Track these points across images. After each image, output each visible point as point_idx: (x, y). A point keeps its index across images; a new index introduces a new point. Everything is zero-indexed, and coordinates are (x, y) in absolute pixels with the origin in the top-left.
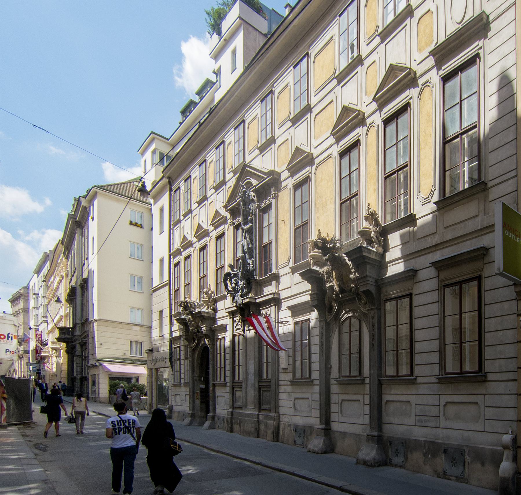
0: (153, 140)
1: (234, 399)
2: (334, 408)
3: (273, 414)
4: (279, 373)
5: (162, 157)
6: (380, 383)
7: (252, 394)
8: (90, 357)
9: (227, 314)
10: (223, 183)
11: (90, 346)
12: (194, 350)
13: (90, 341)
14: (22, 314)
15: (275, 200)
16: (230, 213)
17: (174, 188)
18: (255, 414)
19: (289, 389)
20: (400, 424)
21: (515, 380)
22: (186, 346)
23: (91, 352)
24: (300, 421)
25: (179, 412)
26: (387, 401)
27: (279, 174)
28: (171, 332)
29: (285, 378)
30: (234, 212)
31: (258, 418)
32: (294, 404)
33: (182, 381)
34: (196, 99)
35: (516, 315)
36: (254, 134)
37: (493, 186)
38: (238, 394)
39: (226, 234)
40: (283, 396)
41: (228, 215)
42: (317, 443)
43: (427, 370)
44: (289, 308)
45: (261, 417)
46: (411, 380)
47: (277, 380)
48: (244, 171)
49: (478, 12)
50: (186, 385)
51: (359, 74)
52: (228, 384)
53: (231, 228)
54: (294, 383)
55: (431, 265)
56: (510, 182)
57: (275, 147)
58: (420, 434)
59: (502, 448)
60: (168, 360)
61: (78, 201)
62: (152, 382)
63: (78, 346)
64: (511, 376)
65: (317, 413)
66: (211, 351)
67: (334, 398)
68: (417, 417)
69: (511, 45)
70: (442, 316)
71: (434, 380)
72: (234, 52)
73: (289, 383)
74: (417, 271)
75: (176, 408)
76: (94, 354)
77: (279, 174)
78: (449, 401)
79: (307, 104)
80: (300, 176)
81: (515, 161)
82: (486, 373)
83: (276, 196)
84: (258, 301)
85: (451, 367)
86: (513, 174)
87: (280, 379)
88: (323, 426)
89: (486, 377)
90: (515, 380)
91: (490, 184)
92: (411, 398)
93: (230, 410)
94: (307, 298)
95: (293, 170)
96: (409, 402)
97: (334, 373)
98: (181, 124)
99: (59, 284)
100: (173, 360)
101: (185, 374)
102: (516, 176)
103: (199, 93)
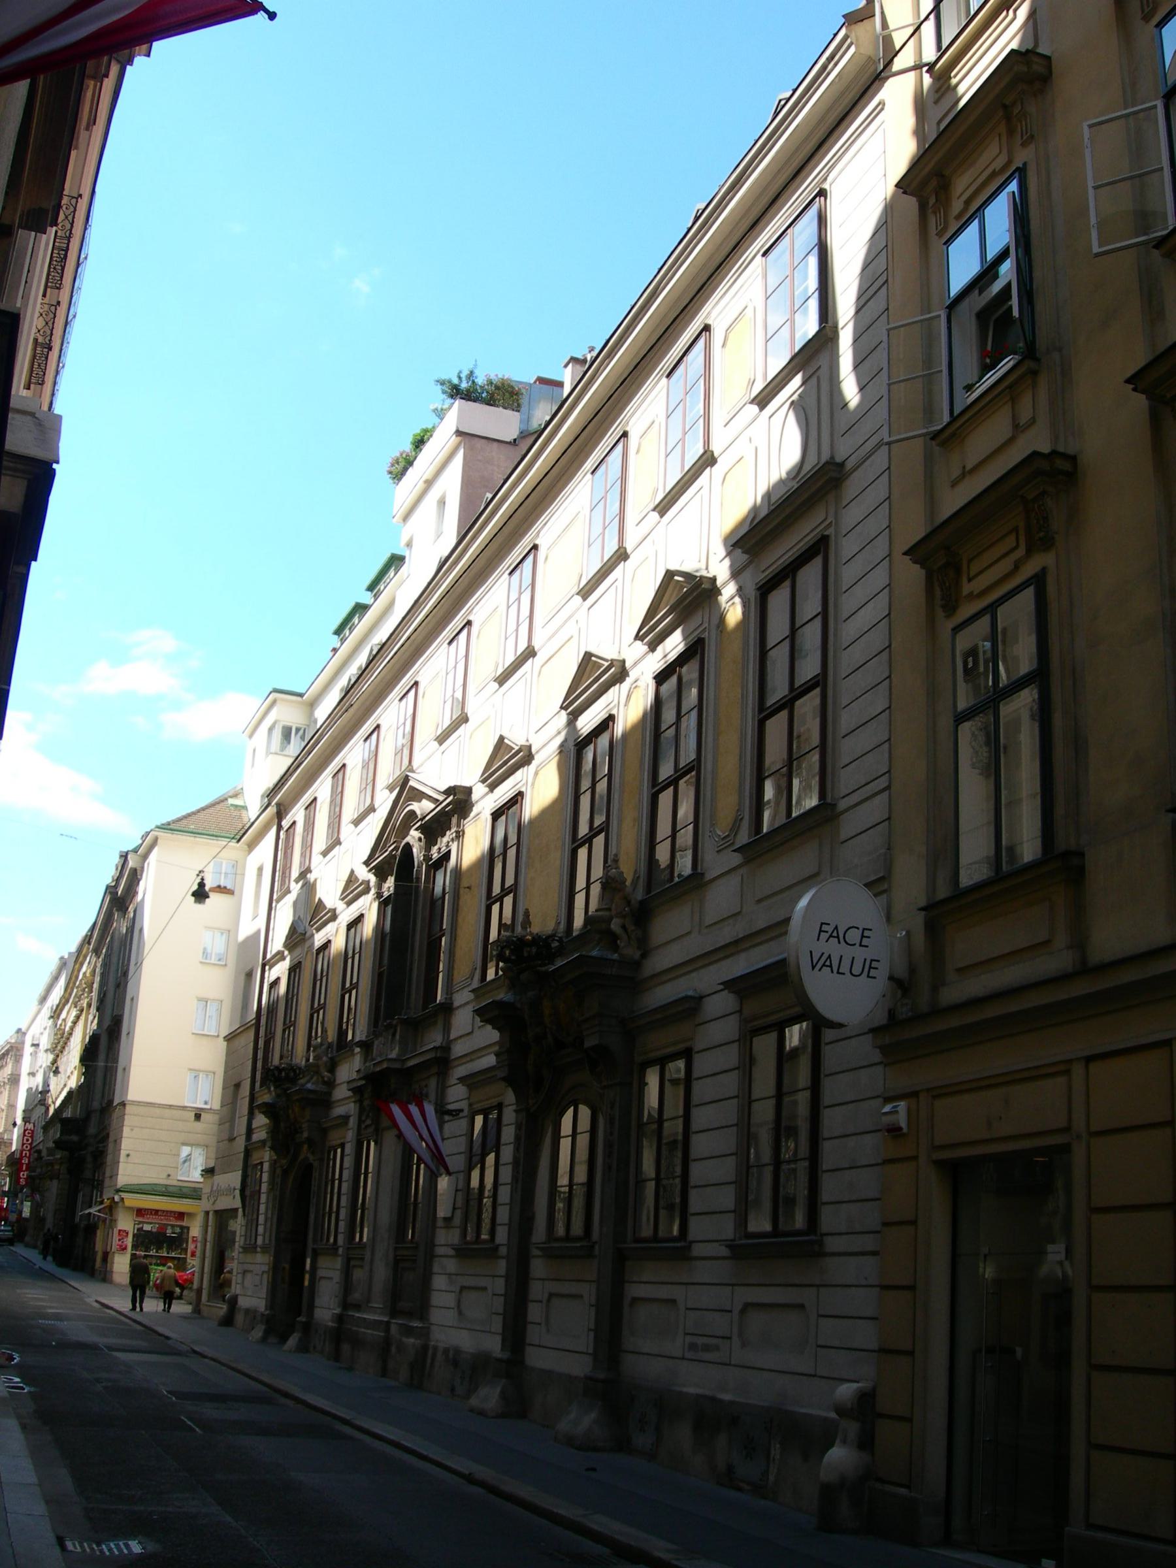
0: (274, 702)
1: (347, 1285)
2: (534, 1312)
3: (416, 1324)
4: (434, 1227)
5: (287, 733)
6: (621, 1259)
7: (382, 1273)
8: (107, 1182)
9: (350, 1093)
10: (371, 809)
11: (109, 1158)
12: (286, 1172)
13: (111, 1146)
14: (8, 1087)
15: (456, 843)
16: (375, 875)
17: (286, 823)
18: (381, 1322)
19: (451, 1265)
20: (660, 1357)
21: (874, 1253)
22: (273, 1164)
23: (108, 1174)
24: (466, 1342)
25: (247, 1311)
26: (635, 1300)
27: (468, 791)
28: (250, 1131)
29: (446, 1239)
30: (381, 873)
31: (387, 1330)
32: (459, 1301)
33: (260, 1241)
34: (367, 598)
35: (881, 1100)
36: (434, 712)
37: (846, 810)
38: (358, 1274)
39: (366, 917)
40: (439, 1282)
41: (373, 879)
42: (489, 1396)
43: (711, 1229)
44: (462, 1080)
45: (394, 1329)
46: (679, 1251)
47: (431, 1245)
48: (405, 789)
49: (825, 457)
50: (265, 1249)
51: (528, 676)
52: (340, 1251)
53: (375, 905)
54: (463, 1252)
55: (721, 987)
56: (877, 800)
57: (718, 470)
58: (695, 1381)
59: (833, 1415)
60: (237, 1192)
61: (124, 856)
62: (206, 1240)
63: (89, 1159)
64: (869, 1242)
65: (497, 1324)
66: (316, 1174)
67: (537, 1290)
68: (689, 1339)
69: (880, 520)
70: (746, 1100)
71: (724, 1251)
72: (442, 503)
73: (452, 1252)
74: (701, 998)
75: (243, 1302)
76: (114, 1175)
77: (468, 791)
78: (750, 1300)
79: (701, 451)
80: (504, 791)
81: (887, 755)
82: (822, 1235)
83: (460, 835)
84: (411, 1063)
85: (760, 1223)
86: (883, 783)
87: (437, 1243)
88: (505, 1355)
89: (821, 1243)
90: (874, 1253)
91: (842, 805)
92: (677, 1293)
93: (338, 1311)
94: (490, 1060)
95: (492, 780)
96: (674, 1301)
97: (539, 1233)
98: (335, 650)
99: (75, 1023)
100: (248, 1193)
101: (265, 1225)
102: (888, 788)
103: (371, 588)
